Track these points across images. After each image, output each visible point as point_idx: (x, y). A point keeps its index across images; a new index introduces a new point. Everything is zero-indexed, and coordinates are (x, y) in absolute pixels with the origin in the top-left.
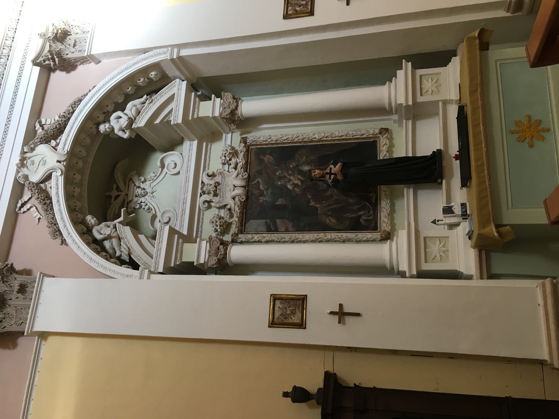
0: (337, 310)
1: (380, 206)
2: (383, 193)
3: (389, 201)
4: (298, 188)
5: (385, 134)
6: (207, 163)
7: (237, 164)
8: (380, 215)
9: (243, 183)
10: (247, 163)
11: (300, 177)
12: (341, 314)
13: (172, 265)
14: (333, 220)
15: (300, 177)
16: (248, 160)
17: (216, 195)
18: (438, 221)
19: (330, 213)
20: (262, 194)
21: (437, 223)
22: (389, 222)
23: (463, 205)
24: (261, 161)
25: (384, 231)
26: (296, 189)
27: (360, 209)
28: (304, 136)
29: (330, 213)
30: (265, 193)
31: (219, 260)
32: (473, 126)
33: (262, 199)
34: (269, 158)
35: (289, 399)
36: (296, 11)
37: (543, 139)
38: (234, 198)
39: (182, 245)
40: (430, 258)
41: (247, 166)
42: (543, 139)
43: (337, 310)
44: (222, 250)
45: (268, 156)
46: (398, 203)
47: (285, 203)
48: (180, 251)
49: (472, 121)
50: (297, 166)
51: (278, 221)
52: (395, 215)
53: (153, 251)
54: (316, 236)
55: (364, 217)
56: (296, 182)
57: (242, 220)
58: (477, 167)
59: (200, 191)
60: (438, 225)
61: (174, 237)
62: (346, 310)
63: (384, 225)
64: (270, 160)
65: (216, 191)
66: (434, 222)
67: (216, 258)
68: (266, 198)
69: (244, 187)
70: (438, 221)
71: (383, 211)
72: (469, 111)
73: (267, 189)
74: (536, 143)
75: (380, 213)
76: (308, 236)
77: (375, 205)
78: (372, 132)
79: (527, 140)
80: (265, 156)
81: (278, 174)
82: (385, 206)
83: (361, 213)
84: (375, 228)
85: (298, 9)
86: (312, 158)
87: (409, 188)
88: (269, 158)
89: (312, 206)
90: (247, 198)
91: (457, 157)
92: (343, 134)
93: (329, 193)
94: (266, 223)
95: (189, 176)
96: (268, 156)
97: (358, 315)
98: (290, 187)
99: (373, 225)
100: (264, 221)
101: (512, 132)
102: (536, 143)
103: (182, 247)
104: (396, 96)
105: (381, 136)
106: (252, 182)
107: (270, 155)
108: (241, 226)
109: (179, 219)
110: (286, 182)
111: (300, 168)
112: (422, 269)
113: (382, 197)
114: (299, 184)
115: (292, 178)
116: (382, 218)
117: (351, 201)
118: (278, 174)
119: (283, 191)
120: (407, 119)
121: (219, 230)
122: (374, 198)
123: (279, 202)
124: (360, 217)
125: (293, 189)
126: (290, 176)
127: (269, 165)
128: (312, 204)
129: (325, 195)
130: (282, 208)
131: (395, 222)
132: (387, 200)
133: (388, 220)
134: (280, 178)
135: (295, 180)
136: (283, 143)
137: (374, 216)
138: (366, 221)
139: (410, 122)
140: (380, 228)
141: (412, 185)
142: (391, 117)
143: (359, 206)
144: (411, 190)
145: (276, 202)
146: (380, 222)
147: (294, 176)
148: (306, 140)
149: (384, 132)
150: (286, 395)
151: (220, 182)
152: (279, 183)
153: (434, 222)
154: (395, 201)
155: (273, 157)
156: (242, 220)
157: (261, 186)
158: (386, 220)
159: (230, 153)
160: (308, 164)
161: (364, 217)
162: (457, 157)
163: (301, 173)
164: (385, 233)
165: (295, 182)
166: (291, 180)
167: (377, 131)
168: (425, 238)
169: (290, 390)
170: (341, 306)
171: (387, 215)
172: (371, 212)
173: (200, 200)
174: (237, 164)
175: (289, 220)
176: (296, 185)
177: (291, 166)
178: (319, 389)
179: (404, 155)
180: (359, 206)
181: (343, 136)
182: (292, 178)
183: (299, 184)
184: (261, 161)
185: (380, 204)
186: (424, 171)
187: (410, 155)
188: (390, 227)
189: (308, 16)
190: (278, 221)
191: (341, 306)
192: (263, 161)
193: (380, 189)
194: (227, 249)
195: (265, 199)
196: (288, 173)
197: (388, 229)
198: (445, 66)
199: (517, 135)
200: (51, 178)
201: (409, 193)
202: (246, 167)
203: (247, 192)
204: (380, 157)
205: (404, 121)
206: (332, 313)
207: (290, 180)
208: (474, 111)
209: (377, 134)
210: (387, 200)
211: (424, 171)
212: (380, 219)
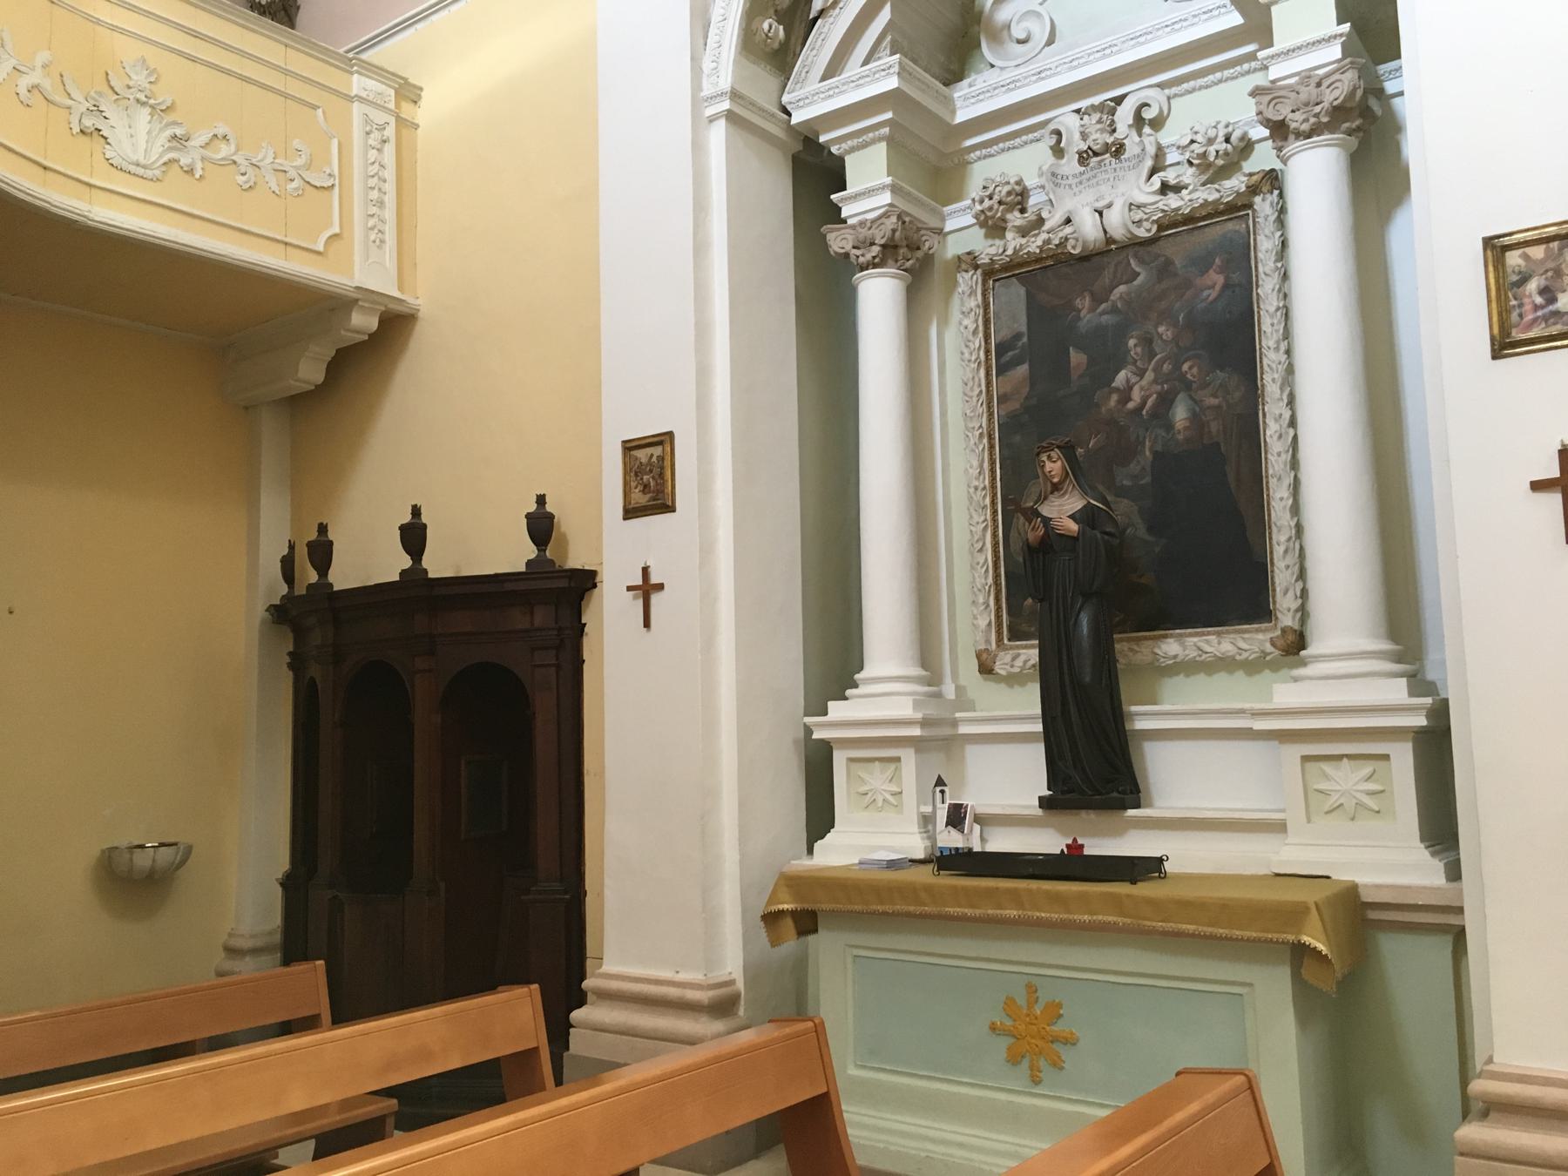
0: (654, 580)
4: (1119, 402)
6: (1192, 83)
7: (1177, 189)
9: (1118, 232)
10: (1189, 219)
11: (1150, 403)
12: (647, 589)
13: (822, 139)
15: (1150, 403)
16: (1204, 218)
17: (1083, 158)
18: (942, 792)
20: (1098, 300)
23: (1149, 868)
24: (1203, 263)
26: (1115, 397)
30: (1103, 306)
31: (847, 255)
32: (1016, 890)
33: (1083, 303)
34: (1213, 287)
35: (533, 507)
36: (1524, 279)
37: (1014, 1059)
38: (1068, 221)
39: (880, 139)
40: (854, 766)
41: (1184, 224)
42: (1014, 1059)
43: (654, 580)
44: (869, 257)
45: (1220, 280)
47: (1074, 376)
48: (862, 141)
49: (1030, 891)
50: (1188, 386)
51: (1023, 370)
53: (853, 68)
56: (1136, 395)
57: (1021, 265)
59: (1083, 104)
61: (884, 111)
62: (655, 599)
65: (1096, 154)
66: (940, 782)
67: (848, 247)
68: (1088, 314)
69: (1109, 240)
70: (942, 792)
72: (1144, 889)
73: (1114, 310)
74: (1004, 1043)
79: (1009, 1023)
80: (1221, 271)
81: (1161, 329)
85: (1533, 286)
86: (1214, 427)
90: (1085, 258)
91: (1075, 848)
94: (1018, 336)
95: (1119, 52)
97: (647, 624)
98: (1121, 378)
99: (1024, 627)
100: (1024, 329)
101: (1032, 990)
102: (1004, 1043)
103: (873, 142)
104: (1311, 678)
106: (1136, 256)
107: (1226, 286)
108: (1006, 267)
109: (1021, 70)
111: (1181, 396)
114: (1131, 405)
115: (1149, 376)
119: (1108, 357)
121: (1212, 150)
123: (1077, 358)
125: (1117, 390)
126: (1154, 370)
127: (1189, 293)
134: (1147, 342)
135: (1142, 389)
145: (1079, 348)
147: (1155, 381)
150: (541, 500)
151: (1126, 156)
153: (940, 782)
155: (1219, 296)
156: (1021, 265)
157: (1122, 288)
159: (1204, 155)
160: (1195, 418)
162: (1075, 848)
163: (1166, 401)
165: (1136, 389)
168: (898, 759)
169: (549, 508)
170: (660, 587)
173: (1066, 118)
174: (1177, 189)
176: (1126, 395)
177: (1185, 367)
178: (426, 571)
182: (1149, 376)
183: (1131, 405)
184: (1203, 263)
186: (1093, 760)
187: (1039, 728)
189: (1493, 339)
190: (1023, 370)
191: (660, 587)
193: (1032, 647)
194: (875, 266)
195: (1082, 314)
196: (1163, 361)
197: (1000, 668)
198: (1422, 840)
199: (1021, 1001)
202: (1170, 224)
203: (1101, 254)
204: (1121, 640)
206: (1537, 486)
207: (1141, 374)
208: (1116, 903)
211: (1093, 760)
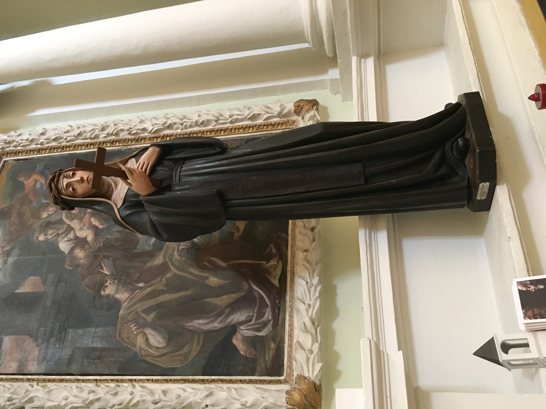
1: (292, 297)
2: (300, 255)
3: (316, 280)
4: (83, 248)
5: (308, 111)
8: (291, 325)
14: (156, 340)
18: (506, 347)
19: (150, 318)
21: (502, 356)
22: (316, 346)
25: (301, 378)
26: (80, 254)
27: (234, 307)
28: (121, 127)
29: (150, 318)
46: (344, 288)
52: (337, 325)
54: (85, 395)
55: (245, 331)
58: (288, 367)
60: (509, 365)
63: (300, 356)
64: (38, 186)
66: (487, 352)
70: (506, 347)
71: (298, 311)
75: (291, 316)
76: (65, 393)
77: (279, 292)
78: (277, 109)
82: (304, 293)
83: (239, 317)
84: (275, 368)
87: (373, 228)
88: (36, 181)
89: (108, 296)
92: (210, 117)
93: (159, 260)
96: (35, 177)
98: (64, 246)
99: (270, 355)
105: (300, 118)
107: (42, 173)
110: (58, 235)
112: (300, 127)
113: (299, 269)
114: (90, 238)
115: (75, 224)
116: (296, 332)
117: (214, 281)
118: (45, 215)
120: (364, 55)
122: (279, 272)
124: (233, 329)
125: (72, 249)
127: (31, 197)
128: (110, 290)
129: (149, 264)
130: (28, 303)
131: (337, 347)
132: (312, 277)
133: (315, 340)
134: (48, 225)
135: (81, 229)
136: (76, 147)
137: (275, 326)
138: (252, 342)
139: (370, 63)
140: (290, 367)
141: (384, 219)
142: (325, 77)
143: (234, 296)
144: (382, 238)
146: (290, 346)
148: (124, 135)
149: (306, 108)
152: (42, 238)
153: (487, 352)
154: (335, 282)
158: (306, 340)
161: (245, 331)
164: (304, 387)
166: (73, 229)
167: (290, 107)
171: (309, 324)
172: (268, 315)
175: (36, 340)
176: (80, 242)
179: (355, 119)
180: (234, 296)
181: (208, 122)
183: (90, 238)
185: (292, 290)
187: (372, 117)
188: (318, 366)
192: (21, 186)
197: (313, 371)
200: (42, 284)
201: (372, 244)
205: (354, 59)
207: (70, 229)
209: (288, 114)
210: (312, 277)
212: (291, 336)
